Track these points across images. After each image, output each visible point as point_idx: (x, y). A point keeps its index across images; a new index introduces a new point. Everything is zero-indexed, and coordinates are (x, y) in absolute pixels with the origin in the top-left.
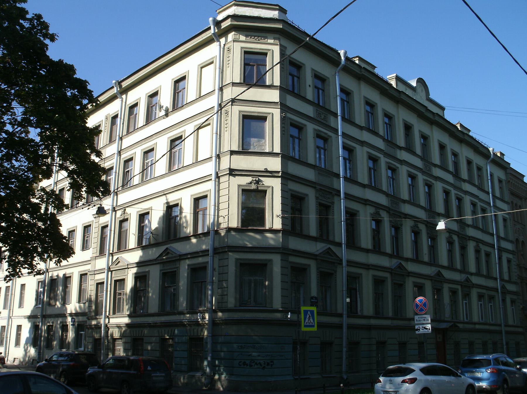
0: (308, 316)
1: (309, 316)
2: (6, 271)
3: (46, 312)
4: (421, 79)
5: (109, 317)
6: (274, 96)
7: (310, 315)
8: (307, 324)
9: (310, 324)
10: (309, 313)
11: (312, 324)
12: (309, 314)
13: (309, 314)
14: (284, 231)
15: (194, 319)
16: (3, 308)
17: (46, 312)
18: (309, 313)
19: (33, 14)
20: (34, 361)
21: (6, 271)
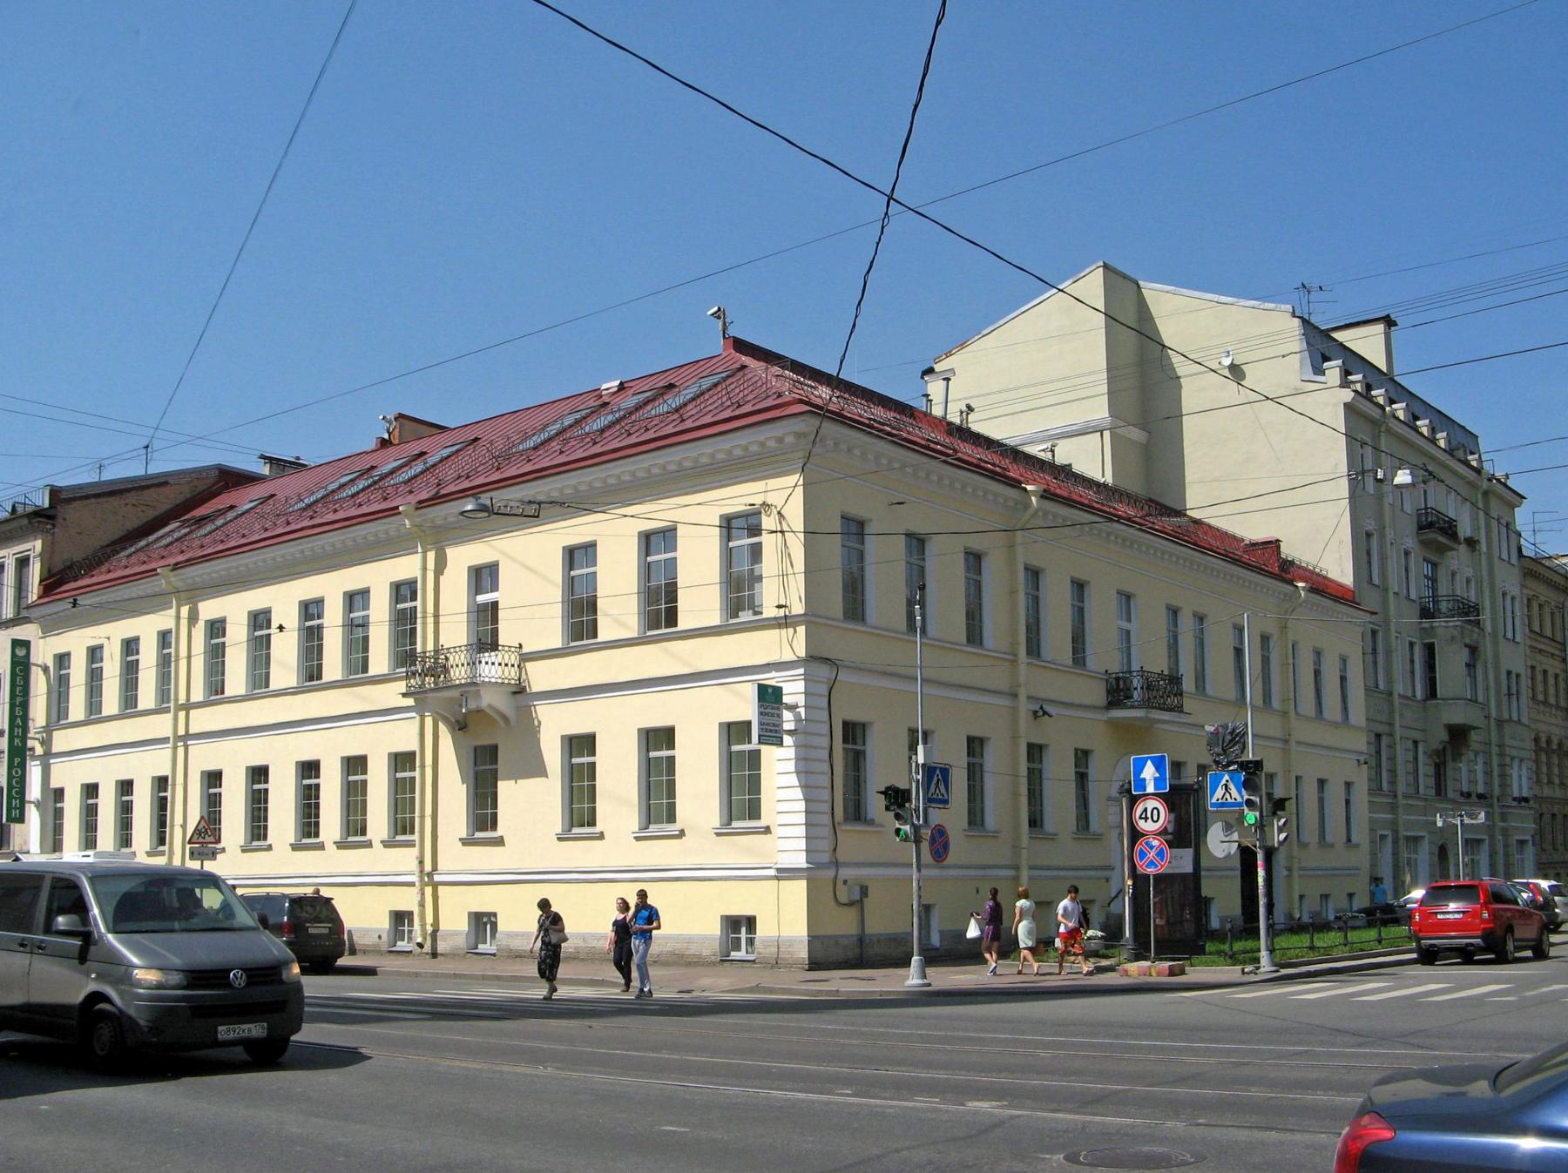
0: (935, 779)
1: (938, 780)
2: (270, 845)
3: (1207, 877)
4: (646, 893)
5: (437, 878)
6: (177, 862)
7: (940, 777)
8: (935, 796)
9: (940, 797)
10: (938, 772)
11: (1233, 801)
12: (938, 775)
13: (938, 775)
14: (543, 913)
15: (47, 524)
16: (503, 848)
17: (1207, 877)
18: (938, 772)
19: (223, 850)
20: (1296, 315)
21: (270, 845)
